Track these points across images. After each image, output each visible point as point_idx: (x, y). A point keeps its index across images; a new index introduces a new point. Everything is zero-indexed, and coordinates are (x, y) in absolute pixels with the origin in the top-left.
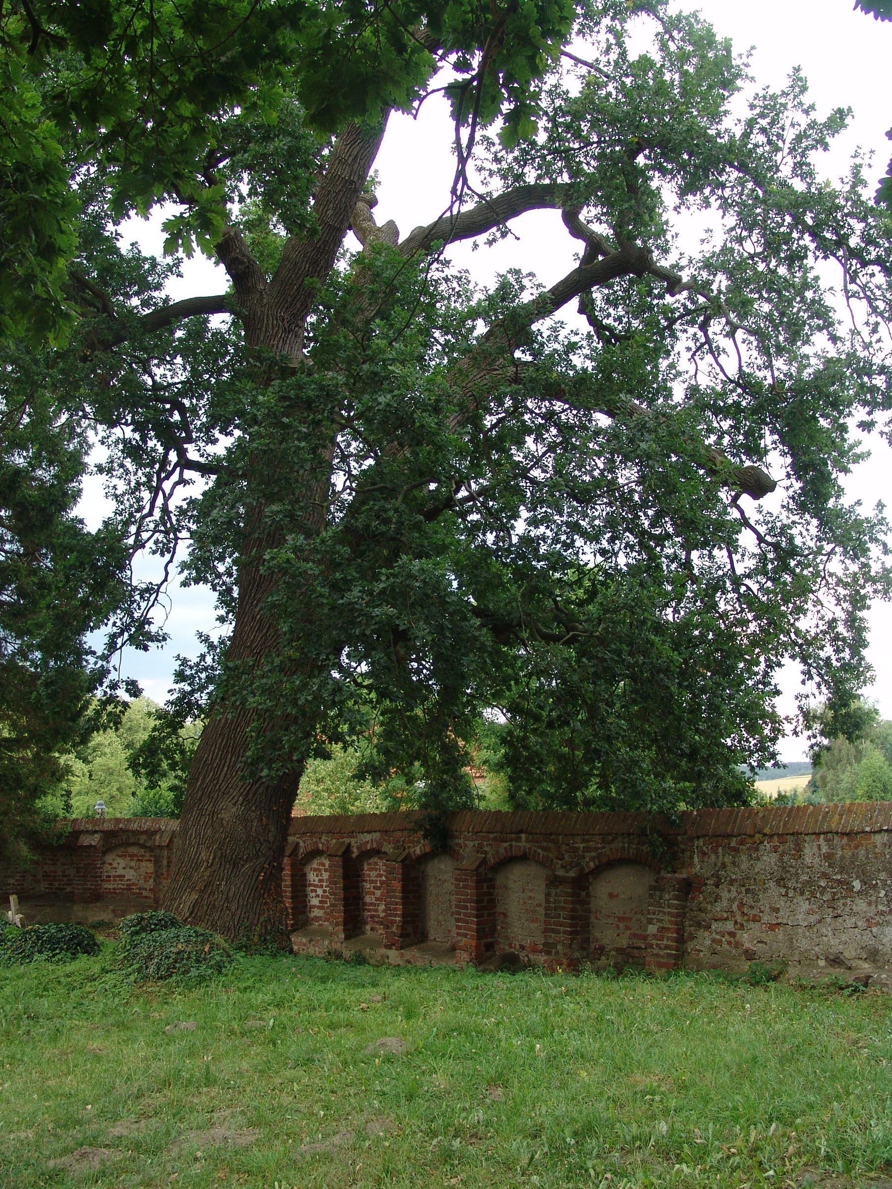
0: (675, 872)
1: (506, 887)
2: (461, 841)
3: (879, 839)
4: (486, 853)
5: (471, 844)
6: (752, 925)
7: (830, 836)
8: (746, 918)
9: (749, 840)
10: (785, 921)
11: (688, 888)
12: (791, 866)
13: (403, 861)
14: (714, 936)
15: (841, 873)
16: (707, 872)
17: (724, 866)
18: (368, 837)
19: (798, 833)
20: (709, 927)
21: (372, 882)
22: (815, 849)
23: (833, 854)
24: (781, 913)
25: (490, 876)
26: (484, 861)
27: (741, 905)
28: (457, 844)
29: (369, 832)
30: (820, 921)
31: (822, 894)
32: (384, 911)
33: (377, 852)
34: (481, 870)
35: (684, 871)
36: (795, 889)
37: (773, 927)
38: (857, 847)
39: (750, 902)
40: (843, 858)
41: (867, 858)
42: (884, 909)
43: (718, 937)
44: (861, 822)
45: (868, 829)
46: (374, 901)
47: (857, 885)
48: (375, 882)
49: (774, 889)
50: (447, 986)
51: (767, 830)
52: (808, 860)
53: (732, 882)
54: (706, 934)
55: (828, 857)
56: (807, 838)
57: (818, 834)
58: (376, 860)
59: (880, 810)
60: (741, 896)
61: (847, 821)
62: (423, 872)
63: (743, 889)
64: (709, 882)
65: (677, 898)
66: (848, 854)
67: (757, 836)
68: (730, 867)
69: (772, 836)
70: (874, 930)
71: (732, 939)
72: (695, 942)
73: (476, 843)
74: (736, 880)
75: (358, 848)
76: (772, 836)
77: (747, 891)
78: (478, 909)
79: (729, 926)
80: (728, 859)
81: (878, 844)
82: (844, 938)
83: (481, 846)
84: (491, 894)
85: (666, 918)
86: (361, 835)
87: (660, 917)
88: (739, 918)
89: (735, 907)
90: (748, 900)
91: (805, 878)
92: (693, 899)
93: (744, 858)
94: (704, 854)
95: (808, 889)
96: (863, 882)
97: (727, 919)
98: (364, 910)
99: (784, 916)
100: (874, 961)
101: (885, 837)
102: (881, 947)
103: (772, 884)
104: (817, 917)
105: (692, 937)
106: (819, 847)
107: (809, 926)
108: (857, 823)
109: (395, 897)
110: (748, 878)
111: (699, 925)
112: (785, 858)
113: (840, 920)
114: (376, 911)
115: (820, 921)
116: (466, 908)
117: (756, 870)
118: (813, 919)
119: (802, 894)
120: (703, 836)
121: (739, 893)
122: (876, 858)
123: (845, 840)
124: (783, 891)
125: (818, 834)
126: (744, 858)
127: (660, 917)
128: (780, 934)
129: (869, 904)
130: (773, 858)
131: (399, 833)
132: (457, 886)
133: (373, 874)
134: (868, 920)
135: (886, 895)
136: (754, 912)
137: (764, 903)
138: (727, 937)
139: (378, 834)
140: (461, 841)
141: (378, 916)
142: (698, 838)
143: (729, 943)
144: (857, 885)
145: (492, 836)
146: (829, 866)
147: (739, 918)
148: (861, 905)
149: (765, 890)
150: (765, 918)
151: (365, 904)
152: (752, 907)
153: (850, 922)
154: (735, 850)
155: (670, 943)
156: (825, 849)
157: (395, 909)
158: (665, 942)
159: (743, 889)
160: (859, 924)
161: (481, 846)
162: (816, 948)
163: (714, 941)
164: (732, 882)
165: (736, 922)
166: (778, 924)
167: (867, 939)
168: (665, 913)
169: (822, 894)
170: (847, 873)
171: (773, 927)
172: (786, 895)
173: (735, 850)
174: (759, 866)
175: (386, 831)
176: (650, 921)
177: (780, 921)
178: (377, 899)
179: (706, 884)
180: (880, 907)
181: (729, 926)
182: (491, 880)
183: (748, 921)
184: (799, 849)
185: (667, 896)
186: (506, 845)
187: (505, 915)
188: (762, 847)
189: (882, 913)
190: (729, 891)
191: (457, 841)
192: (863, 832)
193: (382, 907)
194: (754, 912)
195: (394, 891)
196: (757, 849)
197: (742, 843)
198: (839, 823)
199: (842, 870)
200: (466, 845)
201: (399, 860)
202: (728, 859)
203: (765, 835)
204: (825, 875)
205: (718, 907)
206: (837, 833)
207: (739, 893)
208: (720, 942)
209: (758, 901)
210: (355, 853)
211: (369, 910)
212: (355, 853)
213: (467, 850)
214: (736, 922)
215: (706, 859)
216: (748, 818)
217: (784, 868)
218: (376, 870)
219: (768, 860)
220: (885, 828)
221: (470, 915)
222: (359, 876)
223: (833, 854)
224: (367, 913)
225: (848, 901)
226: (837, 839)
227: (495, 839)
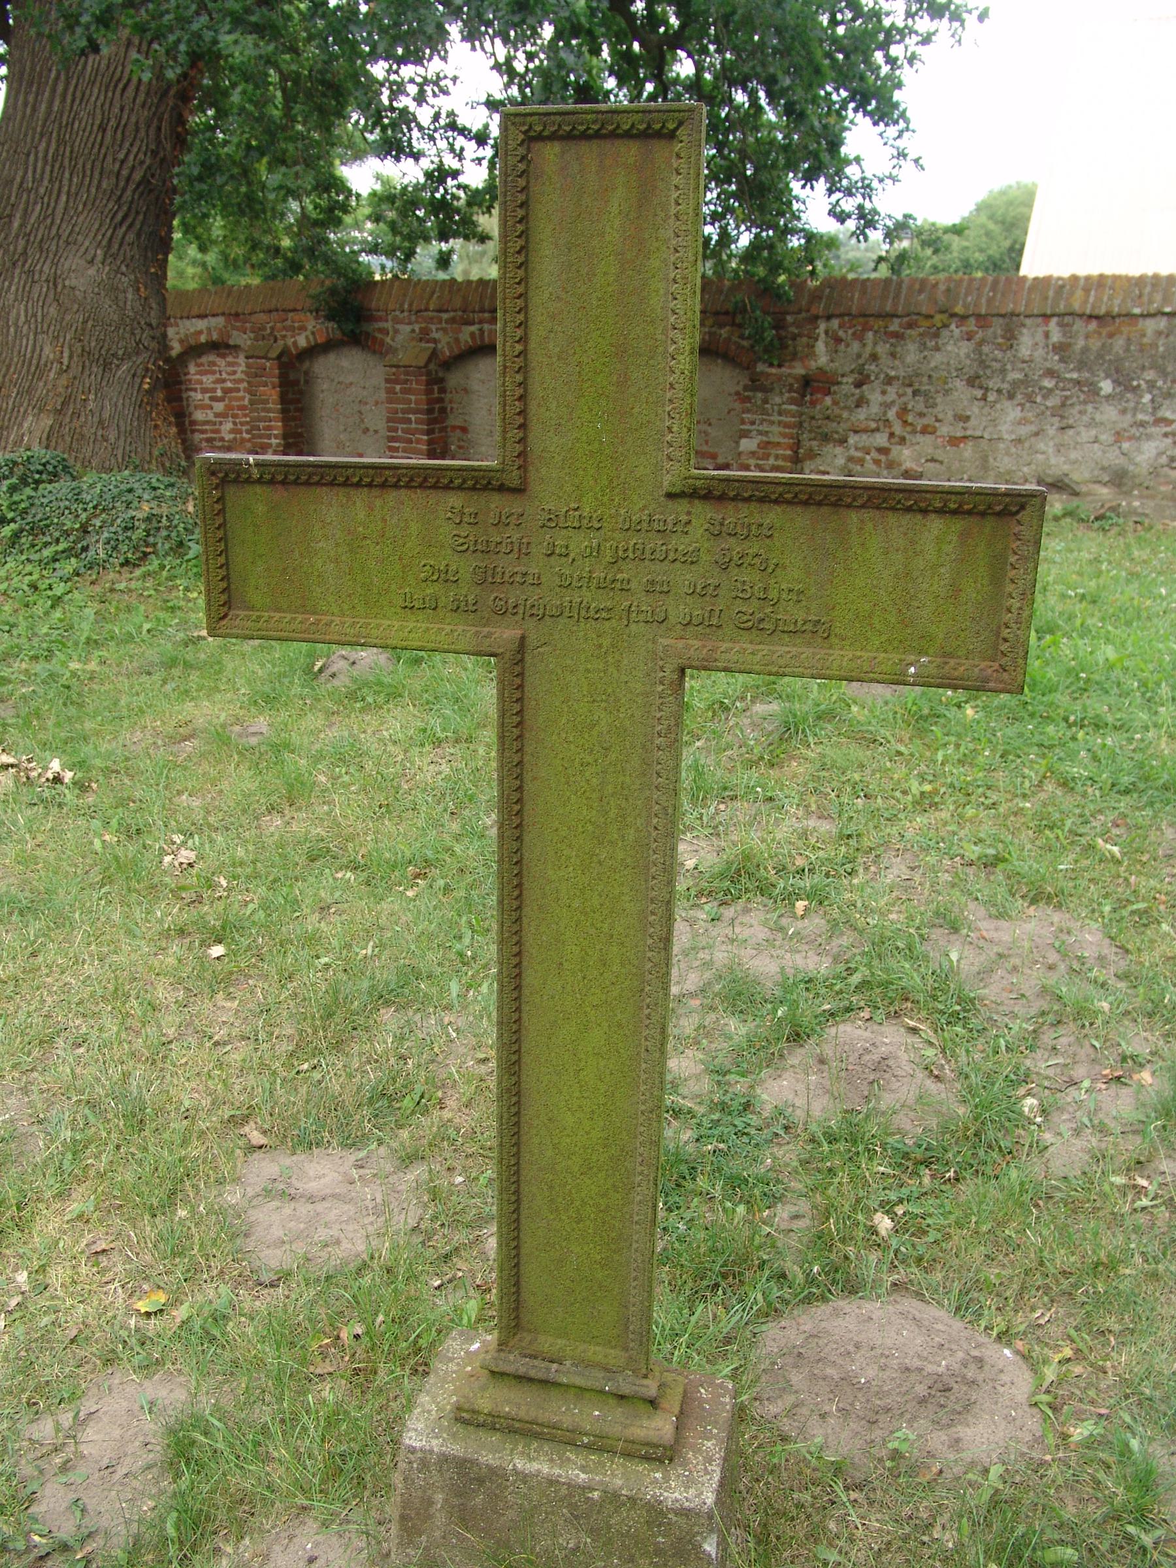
0: (780, 366)
1: (466, 390)
2: (388, 325)
3: (1150, 325)
4: (435, 341)
5: (408, 328)
6: (920, 438)
7: (1067, 319)
8: (909, 429)
9: (925, 323)
10: (979, 433)
11: (812, 386)
12: (996, 360)
13: (279, 357)
14: (852, 452)
15: (1079, 370)
16: (843, 364)
17: (874, 357)
18: (201, 324)
19: (1013, 314)
20: (843, 441)
21: (204, 391)
22: (1039, 337)
23: (1070, 345)
24: (973, 422)
25: (441, 374)
26: (434, 353)
27: (904, 410)
28: (381, 330)
29: (202, 316)
30: (1037, 434)
31: (1045, 397)
32: (231, 431)
33: (219, 347)
34: (432, 366)
35: (797, 364)
36: (999, 391)
37: (954, 441)
38: (1111, 335)
39: (920, 407)
40: (1085, 350)
41: (1127, 350)
42: (1147, 418)
43: (859, 454)
44: (1123, 301)
45: (1137, 311)
46: (211, 417)
47: (1106, 386)
48: (214, 390)
49: (962, 392)
50: (543, 471)
51: (959, 309)
52: (1024, 351)
53: (889, 381)
54: (838, 450)
55: (1060, 348)
56: (1028, 321)
57: (1046, 317)
58: (212, 357)
59: (1153, 285)
60: (904, 399)
61: (1098, 299)
62: (306, 373)
63: (909, 391)
64: (845, 380)
65: (792, 401)
66: (1095, 344)
67: (938, 317)
68: (885, 360)
69: (964, 318)
70: (1126, 445)
71: (883, 458)
72: (818, 460)
73: (417, 327)
74: (897, 378)
75: (181, 341)
76: (964, 318)
77: (915, 393)
78: (430, 422)
79: (881, 440)
80: (882, 349)
81: (1149, 332)
82: (1073, 455)
83: (425, 331)
84: (441, 400)
85: (775, 429)
86: (187, 323)
87: (764, 427)
88: (898, 429)
89: (891, 414)
90: (919, 404)
91: (1018, 376)
92: (813, 403)
93: (912, 347)
94: (838, 340)
95: (1022, 391)
96: (1117, 382)
97: (877, 430)
98: (193, 431)
99: (976, 426)
100: (1119, 486)
101: (1163, 323)
102: (1131, 468)
103: (959, 384)
104: (1033, 428)
105: (812, 455)
106: (1047, 335)
107: (1019, 441)
108: (1117, 302)
109: (269, 411)
110: (918, 375)
111: (826, 438)
112: (986, 349)
113: (1071, 432)
114: (218, 431)
115: (1037, 434)
116: (409, 421)
117: (933, 364)
118: (1024, 431)
119: (1011, 396)
120: (841, 315)
121: (900, 396)
122: (1141, 351)
123: (1093, 325)
124: (979, 393)
125: (1046, 317)
126: (912, 347)
127: (764, 427)
128: (967, 450)
129: (1124, 412)
130: (965, 348)
131: (263, 317)
132: (390, 391)
133: (208, 380)
134: (1118, 433)
135: (1152, 401)
136: (925, 421)
137: (944, 408)
138: (874, 454)
139: (221, 320)
140: (388, 325)
141: (222, 439)
142: (829, 318)
143: (877, 462)
144: (1106, 386)
145: (445, 316)
146: (1062, 360)
147: (898, 429)
148: (1110, 413)
149: (947, 392)
150: (944, 430)
151: (193, 423)
152: (921, 415)
153: (1086, 435)
154: (897, 336)
155: (780, 463)
156: (1056, 337)
157: (269, 428)
158: (771, 461)
159: (909, 391)
160: (1103, 437)
161: (425, 331)
162: (1025, 469)
163: (850, 459)
164: (889, 381)
165: (892, 435)
166: (965, 437)
167: (1113, 458)
168: (772, 423)
169: (1045, 397)
170: (1090, 370)
171: (954, 441)
172: (984, 398)
173: (897, 336)
174: (938, 359)
175: (237, 315)
176: (745, 434)
177: (969, 433)
178: (217, 415)
179: (839, 383)
180: (1140, 417)
181: (881, 440)
182: (442, 380)
183: (914, 432)
184: (1010, 337)
185: (778, 400)
186: (473, 328)
187: (464, 430)
188: (945, 333)
189: (1142, 424)
190: (884, 393)
191: (381, 325)
192: (1129, 315)
193: (229, 426)
194: (925, 421)
195: (266, 402)
196: (936, 335)
197: (910, 326)
198: (1086, 302)
199: (1081, 365)
200: (396, 331)
201: (274, 354)
202: (882, 349)
203: (953, 315)
204: (1050, 373)
205: (861, 414)
206: (1081, 316)
207: (900, 396)
208: (861, 462)
209: (934, 406)
210: (176, 349)
211: (203, 432)
212: (176, 349)
213: (400, 338)
214: (892, 435)
215: (842, 347)
216: (920, 291)
217: (982, 362)
218: (214, 373)
219: (955, 349)
220: (1168, 310)
221: (416, 431)
222: (180, 383)
223: (1070, 345)
224: (198, 437)
225: (1090, 408)
226: (1079, 325)
227: (452, 321)
